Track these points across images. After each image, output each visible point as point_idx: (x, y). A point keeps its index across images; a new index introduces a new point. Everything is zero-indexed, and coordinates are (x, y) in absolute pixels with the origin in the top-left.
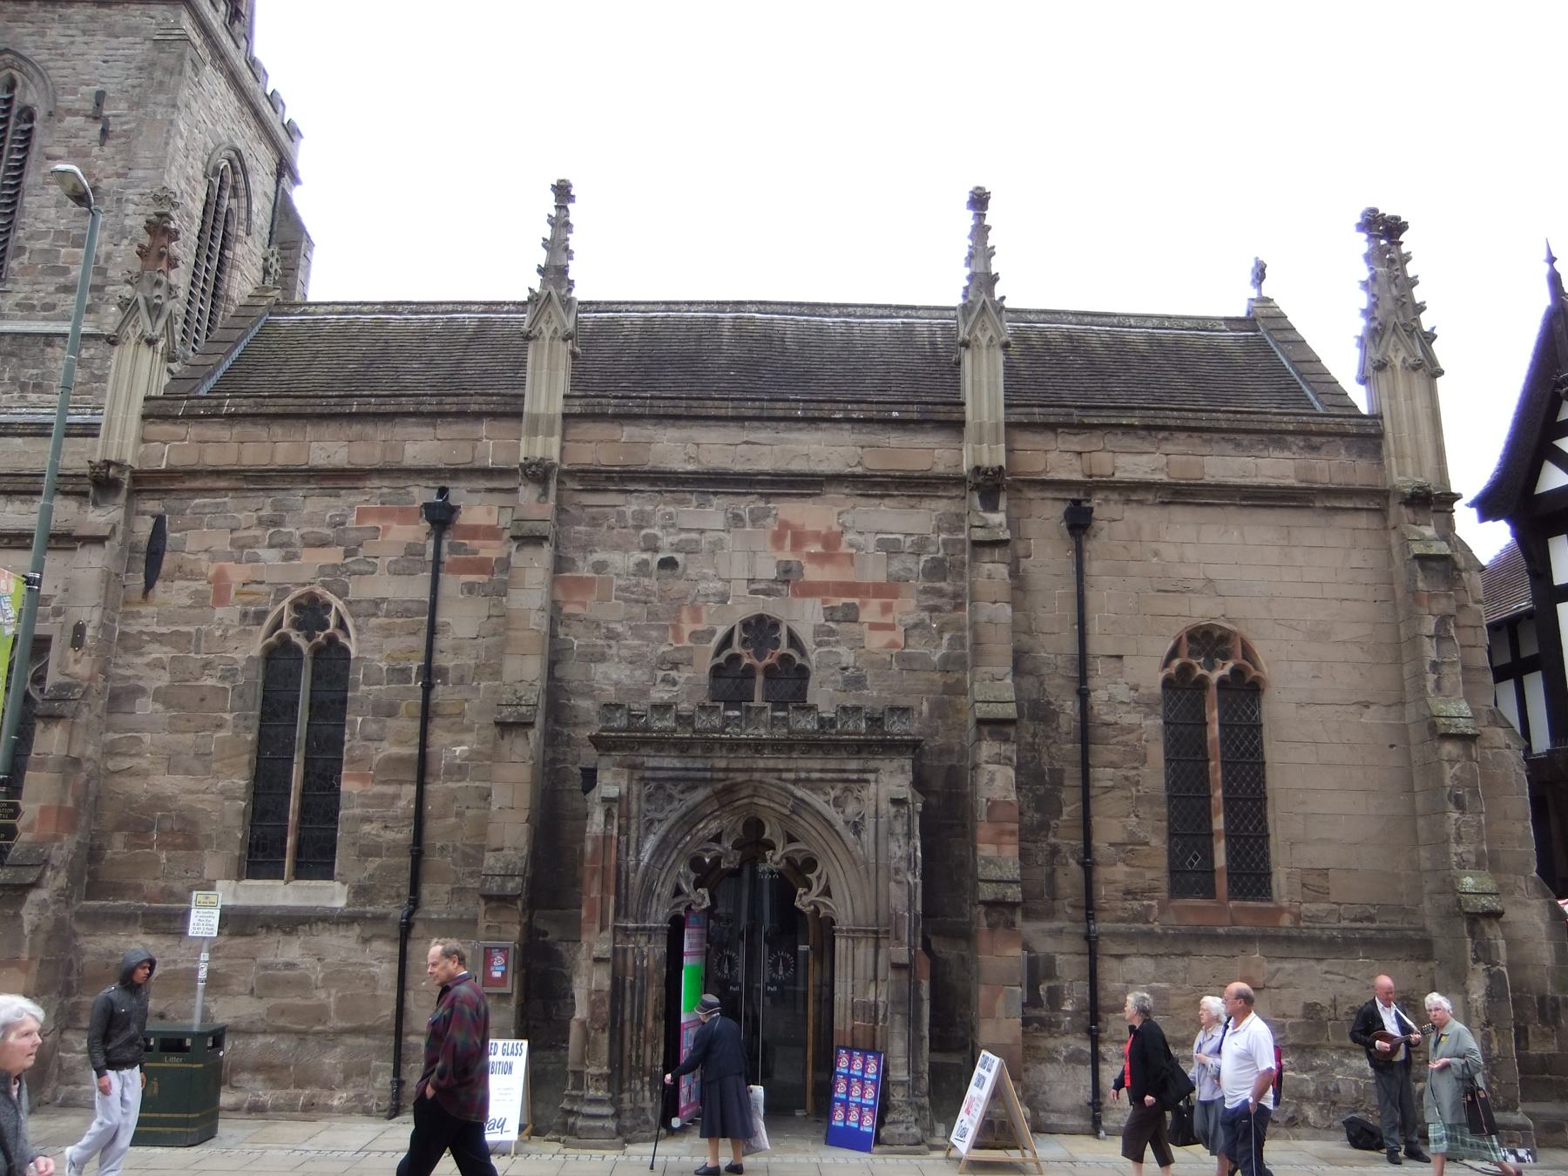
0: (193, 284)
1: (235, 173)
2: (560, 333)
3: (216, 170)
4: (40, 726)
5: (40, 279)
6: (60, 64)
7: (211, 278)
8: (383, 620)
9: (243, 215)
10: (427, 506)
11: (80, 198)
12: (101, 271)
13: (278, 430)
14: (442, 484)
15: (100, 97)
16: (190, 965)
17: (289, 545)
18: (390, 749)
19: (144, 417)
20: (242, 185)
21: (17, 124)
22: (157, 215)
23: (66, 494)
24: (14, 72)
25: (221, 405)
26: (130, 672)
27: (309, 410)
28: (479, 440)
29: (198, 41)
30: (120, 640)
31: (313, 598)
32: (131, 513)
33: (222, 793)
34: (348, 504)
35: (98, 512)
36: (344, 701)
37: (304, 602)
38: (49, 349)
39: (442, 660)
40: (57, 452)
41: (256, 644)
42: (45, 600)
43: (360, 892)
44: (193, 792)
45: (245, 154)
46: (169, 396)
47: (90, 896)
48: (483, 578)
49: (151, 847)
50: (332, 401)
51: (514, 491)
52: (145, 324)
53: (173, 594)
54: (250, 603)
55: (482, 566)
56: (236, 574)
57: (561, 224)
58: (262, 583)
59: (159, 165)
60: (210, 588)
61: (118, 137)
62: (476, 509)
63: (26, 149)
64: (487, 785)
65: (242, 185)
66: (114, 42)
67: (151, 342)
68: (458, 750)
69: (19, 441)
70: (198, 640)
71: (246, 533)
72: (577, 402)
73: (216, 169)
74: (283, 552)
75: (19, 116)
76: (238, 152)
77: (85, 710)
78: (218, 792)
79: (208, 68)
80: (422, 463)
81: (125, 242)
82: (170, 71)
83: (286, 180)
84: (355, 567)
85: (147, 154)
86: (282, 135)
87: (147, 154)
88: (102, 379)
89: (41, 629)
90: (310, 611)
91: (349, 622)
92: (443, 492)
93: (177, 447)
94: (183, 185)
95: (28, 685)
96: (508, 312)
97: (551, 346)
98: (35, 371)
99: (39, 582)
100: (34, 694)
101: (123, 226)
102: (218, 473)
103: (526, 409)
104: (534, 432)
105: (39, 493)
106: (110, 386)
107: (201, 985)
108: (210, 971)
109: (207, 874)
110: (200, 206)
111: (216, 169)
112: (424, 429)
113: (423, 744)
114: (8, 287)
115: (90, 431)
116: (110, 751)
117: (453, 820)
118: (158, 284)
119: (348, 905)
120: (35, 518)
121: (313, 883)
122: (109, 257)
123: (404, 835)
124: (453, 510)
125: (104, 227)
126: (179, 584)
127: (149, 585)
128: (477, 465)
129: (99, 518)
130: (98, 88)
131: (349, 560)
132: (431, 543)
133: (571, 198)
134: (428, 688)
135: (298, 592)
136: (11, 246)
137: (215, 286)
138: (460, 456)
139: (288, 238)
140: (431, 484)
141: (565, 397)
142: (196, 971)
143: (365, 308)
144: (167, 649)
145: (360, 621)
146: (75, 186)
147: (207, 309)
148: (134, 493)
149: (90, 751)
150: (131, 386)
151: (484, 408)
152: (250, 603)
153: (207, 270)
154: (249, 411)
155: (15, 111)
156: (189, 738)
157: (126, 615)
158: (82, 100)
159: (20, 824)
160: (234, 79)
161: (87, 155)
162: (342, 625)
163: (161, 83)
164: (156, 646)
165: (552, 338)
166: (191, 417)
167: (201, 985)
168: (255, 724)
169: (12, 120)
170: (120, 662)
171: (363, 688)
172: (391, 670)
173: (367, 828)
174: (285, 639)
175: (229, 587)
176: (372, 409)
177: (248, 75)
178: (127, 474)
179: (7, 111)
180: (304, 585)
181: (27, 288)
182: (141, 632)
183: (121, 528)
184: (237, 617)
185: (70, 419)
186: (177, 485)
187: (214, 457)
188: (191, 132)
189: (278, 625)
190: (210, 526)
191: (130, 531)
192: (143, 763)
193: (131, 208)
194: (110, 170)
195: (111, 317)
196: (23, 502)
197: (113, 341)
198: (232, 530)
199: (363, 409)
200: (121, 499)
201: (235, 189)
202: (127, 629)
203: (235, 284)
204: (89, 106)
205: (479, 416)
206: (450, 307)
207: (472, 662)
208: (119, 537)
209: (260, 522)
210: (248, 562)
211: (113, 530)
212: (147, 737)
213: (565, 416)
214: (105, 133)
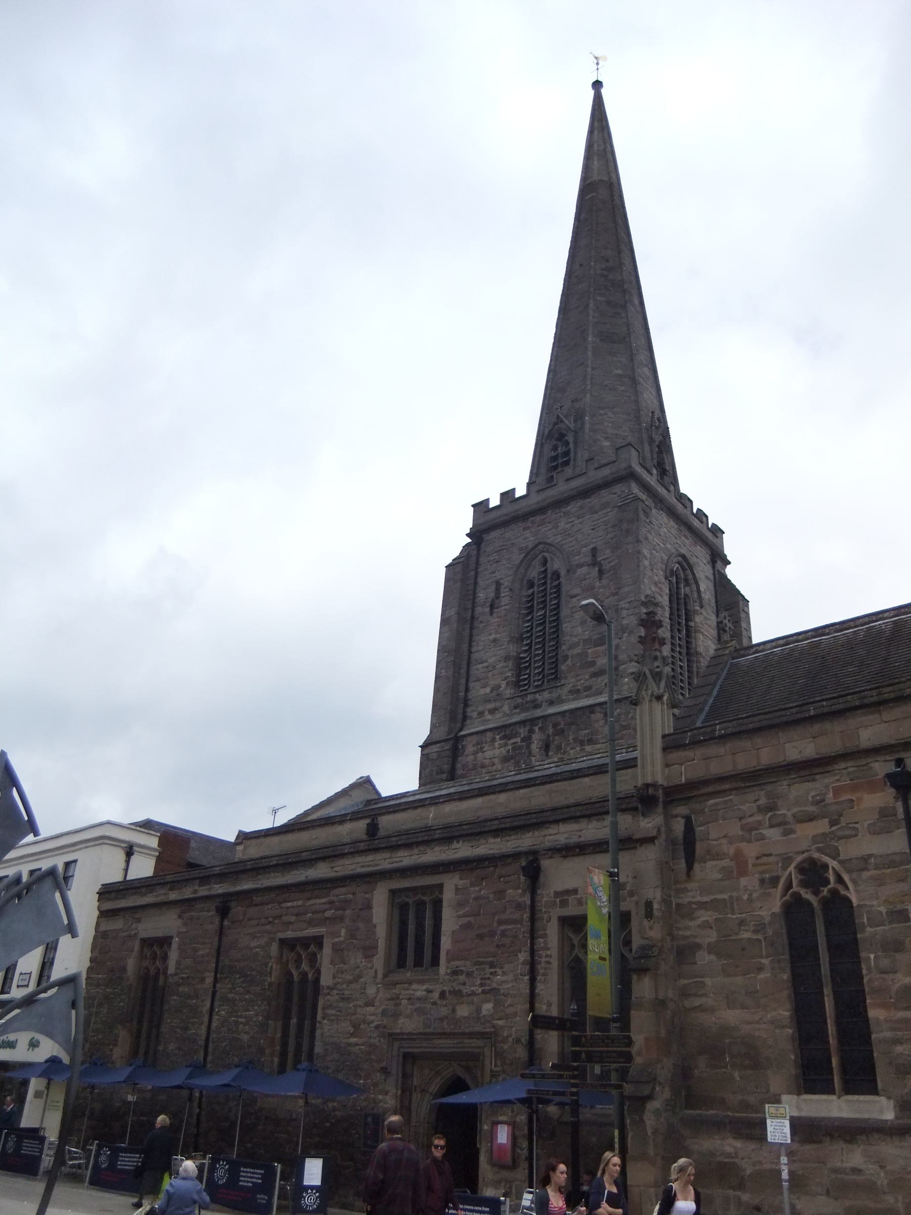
1: (684, 570)
3: (673, 573)
5: (580, 672)
6: (569, 540)
7: (683, 643)
9: (695, 595)
10: (889, 776)
13: (758, 740)
14: (897, 756)
15: (594, 551)
16: (774, 1166)
17: (786, 823)
19: (664, 749)
20: (690, 577)
23: (623, 811)
24: (545, 554)
26: (688, 933)
27: (778, 721)
31: (812, 862)
33: (772, 1023)
35: (646, 820)
36: (855, 941)
37: (806, 865)
40: (614, 780)
41: (775, 904)
44: (750, 1023)
45: (688, 556)
46: (679, 731)
47: (689, 1105)
49: (726, 1067)
52: (653, 687)
53: (708, 871)
54: (764, 872)
56: (751, 856)
58: (771, 855)
61: (609, 571)
63: (559, 596)
65: (690, 577)
66: (596, 516)
67: (659, 698)
69: (587, 779)
70: (732, 904)
71: (751, 819)
73: (672, 571)
74: (781, 829)
77: (663, 963)
78: (768, 1020)
79: (654, 511)
81: (626, 635)
83: (719, 564)
84: (840, 833)
86: (709, 535)
89: (624, 906)
90: (813, 873)
91: (846, 877)
92: (899, 762)
93: (690, 766)
94: (653, 588)
98: (587, 731)
99: (617, 875)
100: (626, 954)
105: (607, 813)
107: (785, 1184)
108: (791, 1173)
109: (773, 1089)
110: (667, 598)
112: (871, 717)
114: (563, 682)
115: (631, 764)
118: (656, 658)
119: (897, 1118)
121: (862, 1098)
126: (710, 864)
127: (690, 867)
129: (648, 824)
130: (592, 546)
131: (834, 828)
135: (800, 858)
137: (688, 648)
139: (732, 604)
140: (888, 758)
142: (779, 1172)
144: (709, 913)
145: (855, 875)
146: (595, 612)
148: (668, 803)
149: (670, 994)
150: (652, 730)
152: (764, 872)
154: (734, 730)
155: (549, 576)
156: (739, 980)
159: (634, 1050)
160: (672, 513)
161: (593, 588)
162: (840, 879)
163: (628, 531)
164: (702, 912)
166: (695, 743)
167: (785, 1184)
168: (787, 965)
169: (549, 581)
170: (680, 925)
171: (869, 929)
172: (891, 913)
174: (797, 896)
176: (826, 710)
177: (679, 507)
178: (660, 791)
180: (803, 852)
181: (573, 680)
182: (690, 903)
183: (663, 829)
184: (756, 883)
186: (695, 793)
187: (716, 768)
188: (652, 554)
189: (789, 886)
190: (724, 819)
191: (669, 830)
192: (709, 1001)
195: (627, 686)
196: (598, 820)
197: (635, 703)
198: (741, 819)
199: (819, 711)
200: (660, 809)
201: (686, 580)
202: (680, 901)
204: (589, 559)
206: (867, 620)
208: (663, 836)
209: (760, 809)
210: (757, 840)
211: (659, 831)
212: (708, 981)
214: (601, 572)
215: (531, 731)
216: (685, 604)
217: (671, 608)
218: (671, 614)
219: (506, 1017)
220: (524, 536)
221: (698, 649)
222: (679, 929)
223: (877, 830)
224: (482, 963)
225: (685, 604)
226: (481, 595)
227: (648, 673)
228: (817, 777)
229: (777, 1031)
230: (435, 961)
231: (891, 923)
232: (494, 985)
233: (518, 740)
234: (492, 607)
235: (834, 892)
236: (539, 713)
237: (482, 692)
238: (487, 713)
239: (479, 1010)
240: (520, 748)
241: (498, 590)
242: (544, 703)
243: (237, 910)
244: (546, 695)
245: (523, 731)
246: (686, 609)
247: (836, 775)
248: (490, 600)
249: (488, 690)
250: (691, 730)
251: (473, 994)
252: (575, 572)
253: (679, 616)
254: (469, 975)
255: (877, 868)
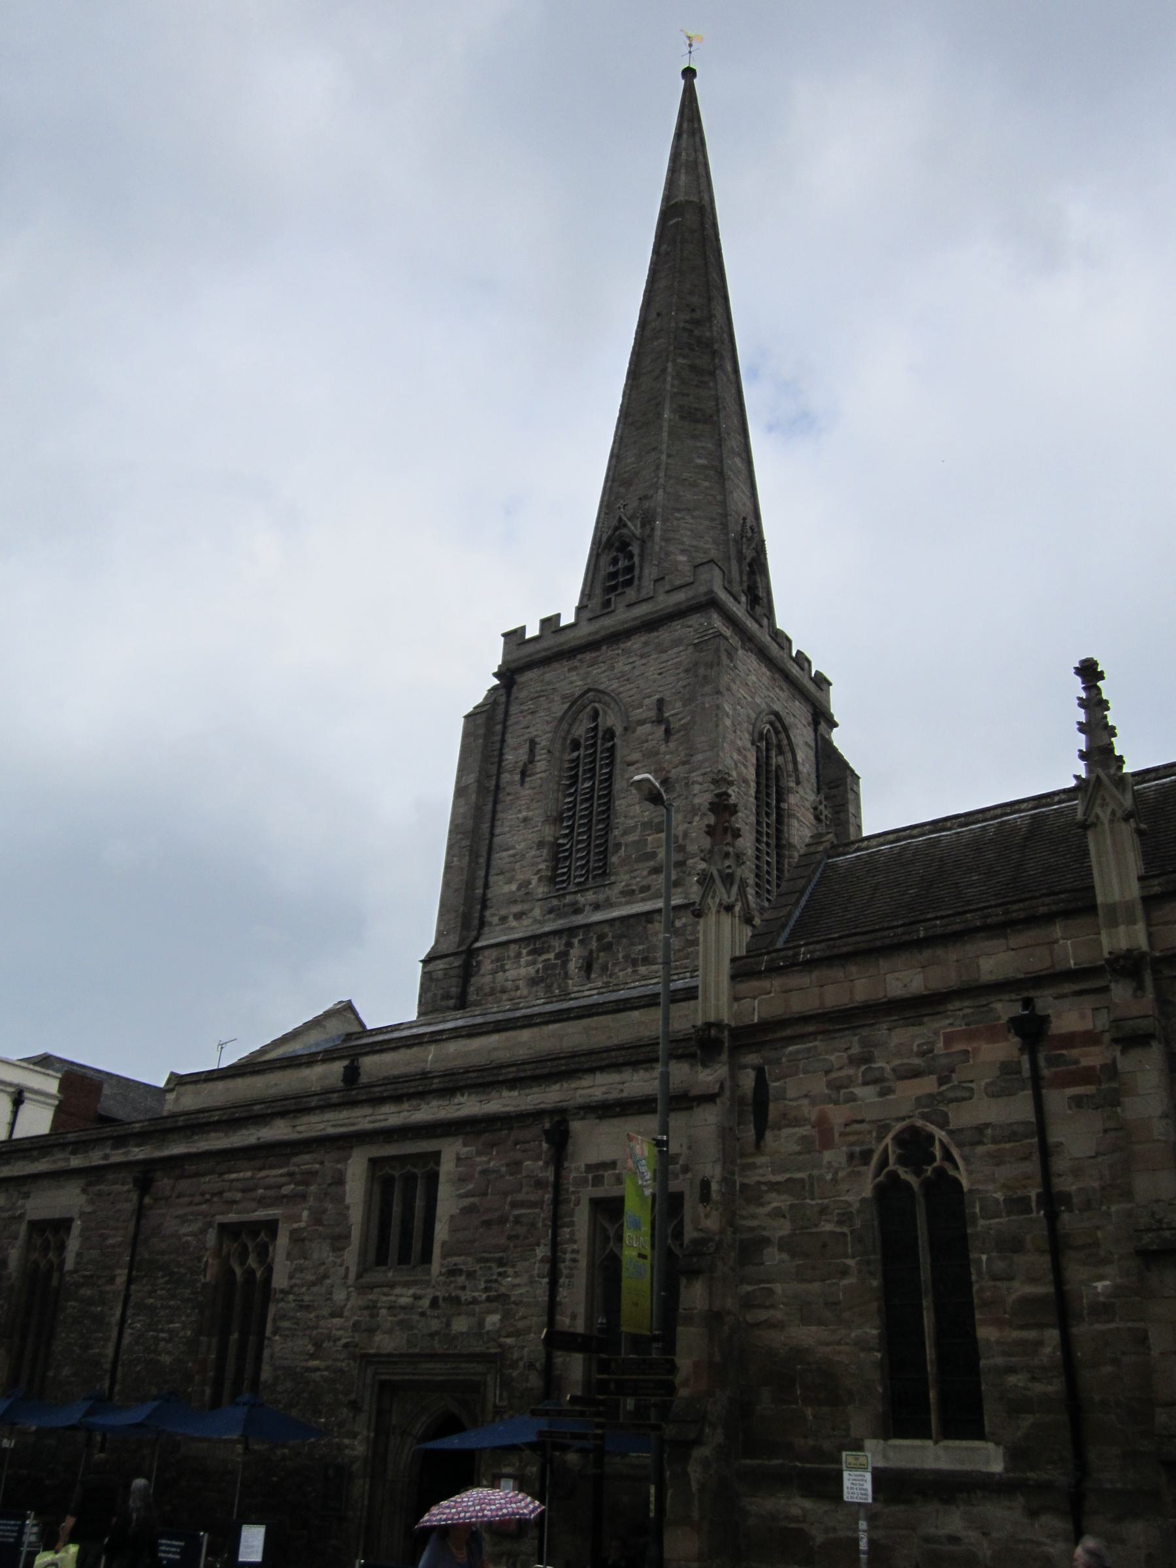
0: (758, 841)
1: (777, 733)
2: (1119, 814)
4: (683, 1282)
5: (636, 867)
7: (772, 831)
8: (991, 1147)
9: (790, 767)
11: (655, 798)
12: (681, 849)
14: (1025, 994)
15: (661, 703)
16: (849, 1534)
18: (1022, 1289)
19: (734, 977)
21: (603, 744)
22: (718, 795)
23: (679, 1058)
24: (596, 705)
25: (798, 954)
26: (755, 1223)
27: (878, 943)
28: (1056, 942)
29: (728, 633)
30: (741, 1192)
31: (913, 1131)
32: (735, 1068)
34: (933, 1031)
35: (708, 1071)
36: (964, 1237)
38: (650, 926)
39: (1066, 1184)
41: (863, 1188)
42: (674, 1159)
43: (1015, 1455)
44: (828, 1344)
45: (783, 714)
46: (753, 951)
48: (1090, 1089)
50: (900, 930)
51: (1105, 989)
52: (722, 894)
53: (784, 1142)
55: (1086, 1076)
56: (840, 1113)
57: (1094, 704)
58: (862, 1121)
59: (714, 746)
60: (814, 1132)
61: (679, 731)
62: (1068, 1016)
64: (1141, 1325)
65: (785, 742)
66: (664, 657)
67: (729, 908)
68: (1100, 1285)
69: (636, 1013)
70: (812, 1185)
72: (1156, 882)
73: (761, 734)
75: (603, 738)
76: (777, 715)
79: (740, 652)
80: (999, 976)
81: (697, 818)
82: (710, 666)
83: (823, 726)
84: (951, 1095)
85: (703, 739)
86: (811, 687)
87: (703, 739)
88: (695, 943)
89: (674, 1186)
90: (914, 1145)
91: (955, 1153)
92: (1028, 1003)
93: (766, 1001)
95: (669, 1241)
96: (1059, 802)
97: (1112, 831)
98: (641, 947)
100: (677, 1251)
101: (693, 805)
102: (805, 1019)
103: (1100, 900)
104: (1113, 923)
105: (656, 1060)
106: (701, 948)
107: (863, 1557)
108: (871, 1542)
110: (752, 770)
111: (761, 734)
112: (995, 942)
113: (1059, 1280)
114: (613, 879)
115: (690, 994)
116: (748, 1303)
117: (1108, 1369)
118: (727, 855)
119: (1006, 1470)
120: (657, 1083)
122: (686, 835)
123: (1054, 1387)
124: (1045, 1020)
125: (678, 811)
126: (786, 1131)
127: (760, 1136)
128: (1058, 968)
129: (707, 1077)
130: (657, 697)
131: (944, 1088)
132: (1025, 1061)
133: (1101, 676)
134: (1052, 1218)
135: (898, 1127)
136: (610, 844)
138: (1038, 962)
139: (837, 781)
140: (1014, 997)
141: (1140, 879)
142: (856, 1541)
143: (915, 832)
144: (783, 1197)
145: (967, 1150)
147: (773, 860)
149: (729, 1303)
150: (718, 951)
151: (1054, 908)
153: (768, 825)
155: (600, 734)
156: (816, 1286)
157: (745, 1168)
158: (646, 711)
159: (678, 1379)
160: (763, 655)
161: (657, 753)
162: (948, 1156)
163: (705, 677)
164: (774, 1195)
165: (1111, 821)
166: (774, 970)
169: (599, 742)
170: (744, 1213)
171: (982, 1222)
172: (1009, 1201)
173: (1012, 1379)
174: (893, 1176)
175: (832, 1129)
176: (939, 931)
177: (774, 647)
178: (726, 1033)
179: (595, 736)
180: (903, 1119)
181: (627, 877)
182: (759, 1183)
183: (728, 1084)
184: (843, 1159)
185: (673, 986)
186: (770, 1037)
187: (800, 1004)
190: (806, 1072)
191: (736, 1086)
192: (778, 1314)
193: (697, 788)
194: (676, 760)
196: (646, 1070)
198: (827, 1072)
199: (931, 932)
202: (746, 1181)
203: (794, 832)
204: (653, 714)
205: (1049, 918)
206: (999, 811)
207: (1096, 1185)
208: (727, 1093)
211: (722, 1087)
212: (778, 1288)
213: (1145, 900)
214: (668, 732)
215: (569, 945)
216: (777, 778)
217: (758, 783)
218: (758, 792)
219: (517, 1333)
220: (568, 680)
221: (791, 841)
222: (744, 1218)
223: (997, 1092)
224: (487, 1260)
225: (777, 778)
226: (509, 757)
227: (715, 873)
228: (926, 1019)
229: (862, 1355)
230: (426, 1258)
231: (1009, 1213)
232: (503, 1290)
233: (551, 956)
234: (523, 774)
235: (940, 1172)
236: (580, 920)
237: (506, 889)
238: (511, 918)
239: (481, 1324)
240: (554, 966)
241: (532, 751)
242: (587, 908)
243: (164, 1184)
244: (590, 896)
245: (558, 944)
246: (777, 786)
247: (948, 1017)
248: (521, 764)
249: (514, 887)
250: (768, 953)
251: (475, 1301)
252: (634, 731)
253: (768, 795)
254: (471, 1275)
255: (995, 1141)
